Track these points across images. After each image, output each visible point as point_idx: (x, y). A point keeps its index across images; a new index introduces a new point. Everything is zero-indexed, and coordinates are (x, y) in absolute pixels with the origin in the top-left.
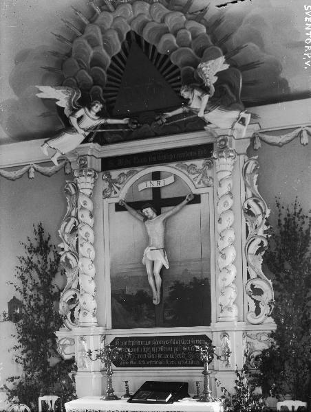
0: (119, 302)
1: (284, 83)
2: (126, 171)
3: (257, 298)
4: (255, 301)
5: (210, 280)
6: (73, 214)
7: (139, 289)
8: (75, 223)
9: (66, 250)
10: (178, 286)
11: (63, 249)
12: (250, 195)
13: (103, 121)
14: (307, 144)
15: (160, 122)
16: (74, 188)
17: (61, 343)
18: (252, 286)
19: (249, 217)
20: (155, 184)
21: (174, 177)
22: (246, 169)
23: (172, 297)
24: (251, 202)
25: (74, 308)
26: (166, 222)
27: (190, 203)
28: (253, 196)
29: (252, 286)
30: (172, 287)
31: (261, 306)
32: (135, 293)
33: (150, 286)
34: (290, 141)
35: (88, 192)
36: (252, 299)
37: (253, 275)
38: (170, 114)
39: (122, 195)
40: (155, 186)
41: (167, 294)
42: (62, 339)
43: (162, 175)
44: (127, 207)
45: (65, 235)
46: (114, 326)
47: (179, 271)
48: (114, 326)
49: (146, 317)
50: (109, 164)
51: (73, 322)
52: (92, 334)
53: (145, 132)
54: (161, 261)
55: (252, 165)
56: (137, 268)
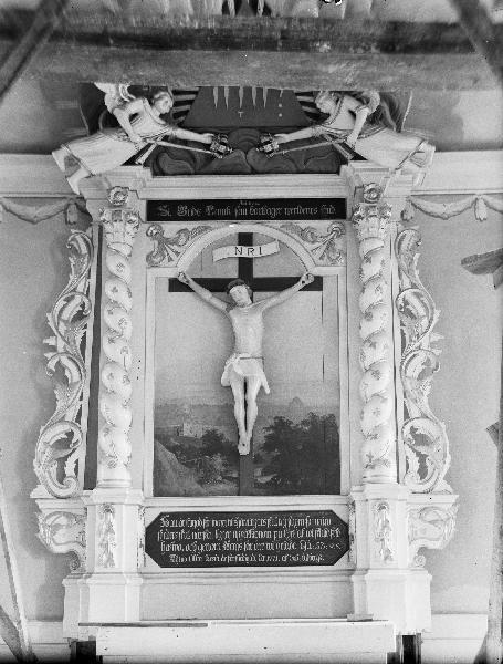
0: (168, 448)
1: (456, 123)
2: (190, 225)
3: (423, 450)
4: (418, 454)
5: (339, 417)
6: (80, 289)
7: (210, 428)
8: (83, 306)
9: (60, 349)
10: (281, 425)
11: (54, 349)
12: (407, 283)
13: (170, 131)
14: (485, 219)
15: (268, 148)
16: (87, 243)
17: (49, 522)
18: (413, 430)
19: (407, 320)
20: (245, 252)
21: (276, 244)
22: (400, 244)
23: (270, 444)
24: (408, 294)
25: (66, 458)
26: (265, 314)
27: (307, 288)
28: (414, 286)
29: (413, 430)
30: (271, 427)
31: (428, 463)
32: (201, 434)
33: (235, 424)
34: (460, 213)
35: (126, 251)
36: (414, 451)
37: (414, 412)
38: (287, 138)
39: (184, 263)
40: (245, 255)
41: (261, 439)
42: (50, 515)
43: (255, 239)
44: (193, 285)
45: (62, 324)
46: (158, 493)
47: (284, 398)
48: (158, 493)
49: (220, 478)
50: (158, 211)
51: (61, 482)
52: (126, 501)
53: (236, 164)
54: (258, 380)
55: (409, 238)
56: (207, 391)
